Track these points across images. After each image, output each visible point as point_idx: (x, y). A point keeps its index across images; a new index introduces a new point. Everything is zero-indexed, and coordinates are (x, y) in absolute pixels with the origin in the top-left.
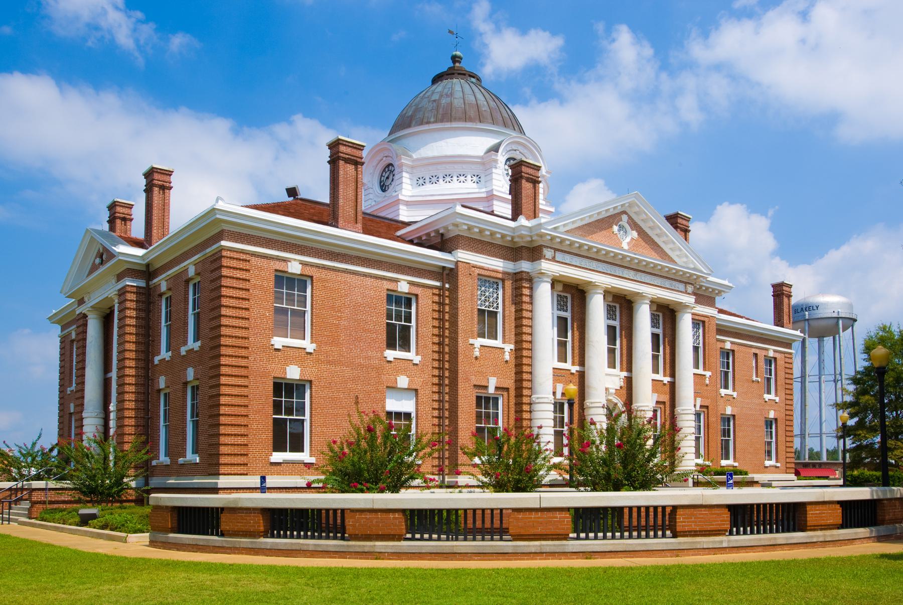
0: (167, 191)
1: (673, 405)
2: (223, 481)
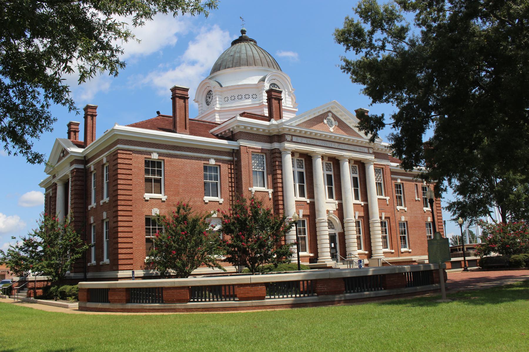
0: (94, 117)
2: (120, 274)
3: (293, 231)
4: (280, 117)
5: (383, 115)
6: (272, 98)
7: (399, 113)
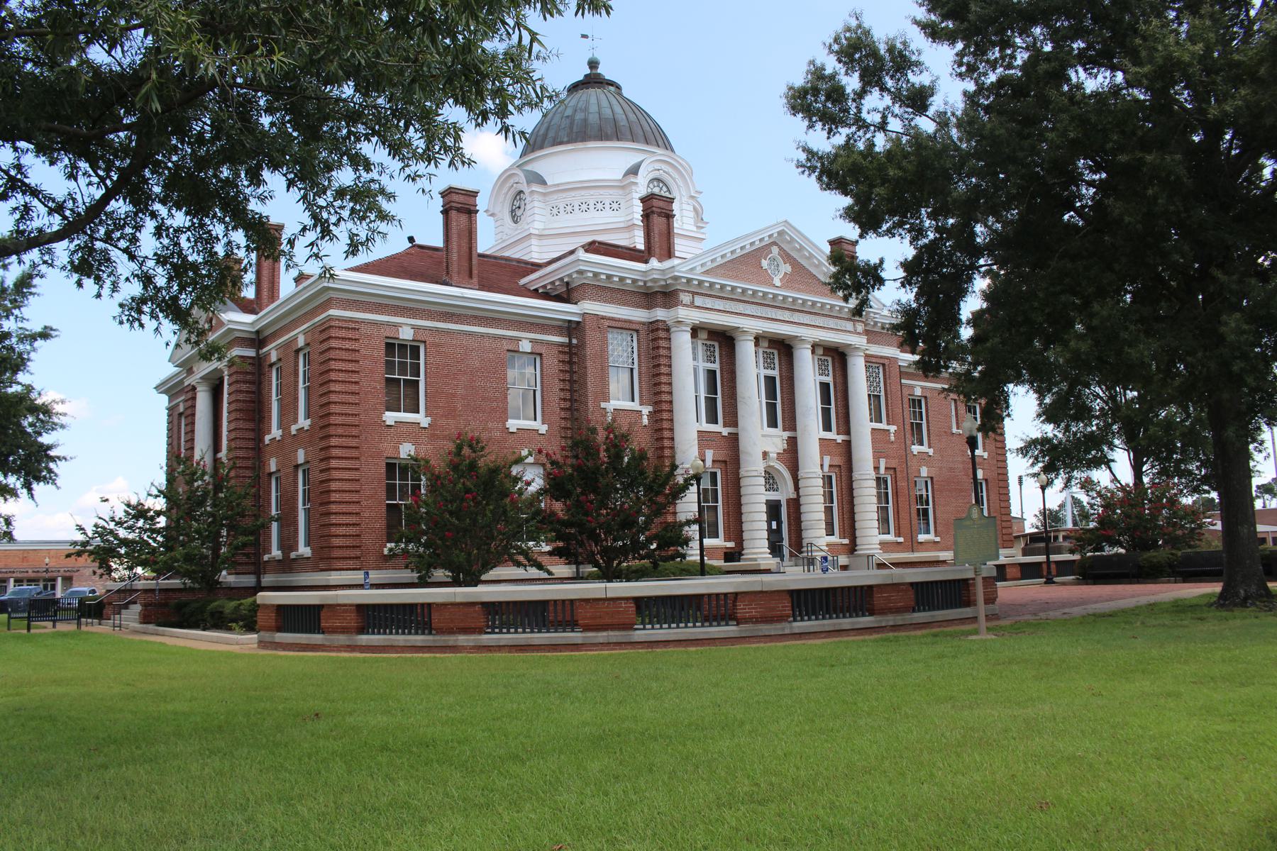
1: (850, 470)
3: (692, 495)
4: (669, 253)
5: (882, 261)
6: (653, 212)
7: (915, 257)
